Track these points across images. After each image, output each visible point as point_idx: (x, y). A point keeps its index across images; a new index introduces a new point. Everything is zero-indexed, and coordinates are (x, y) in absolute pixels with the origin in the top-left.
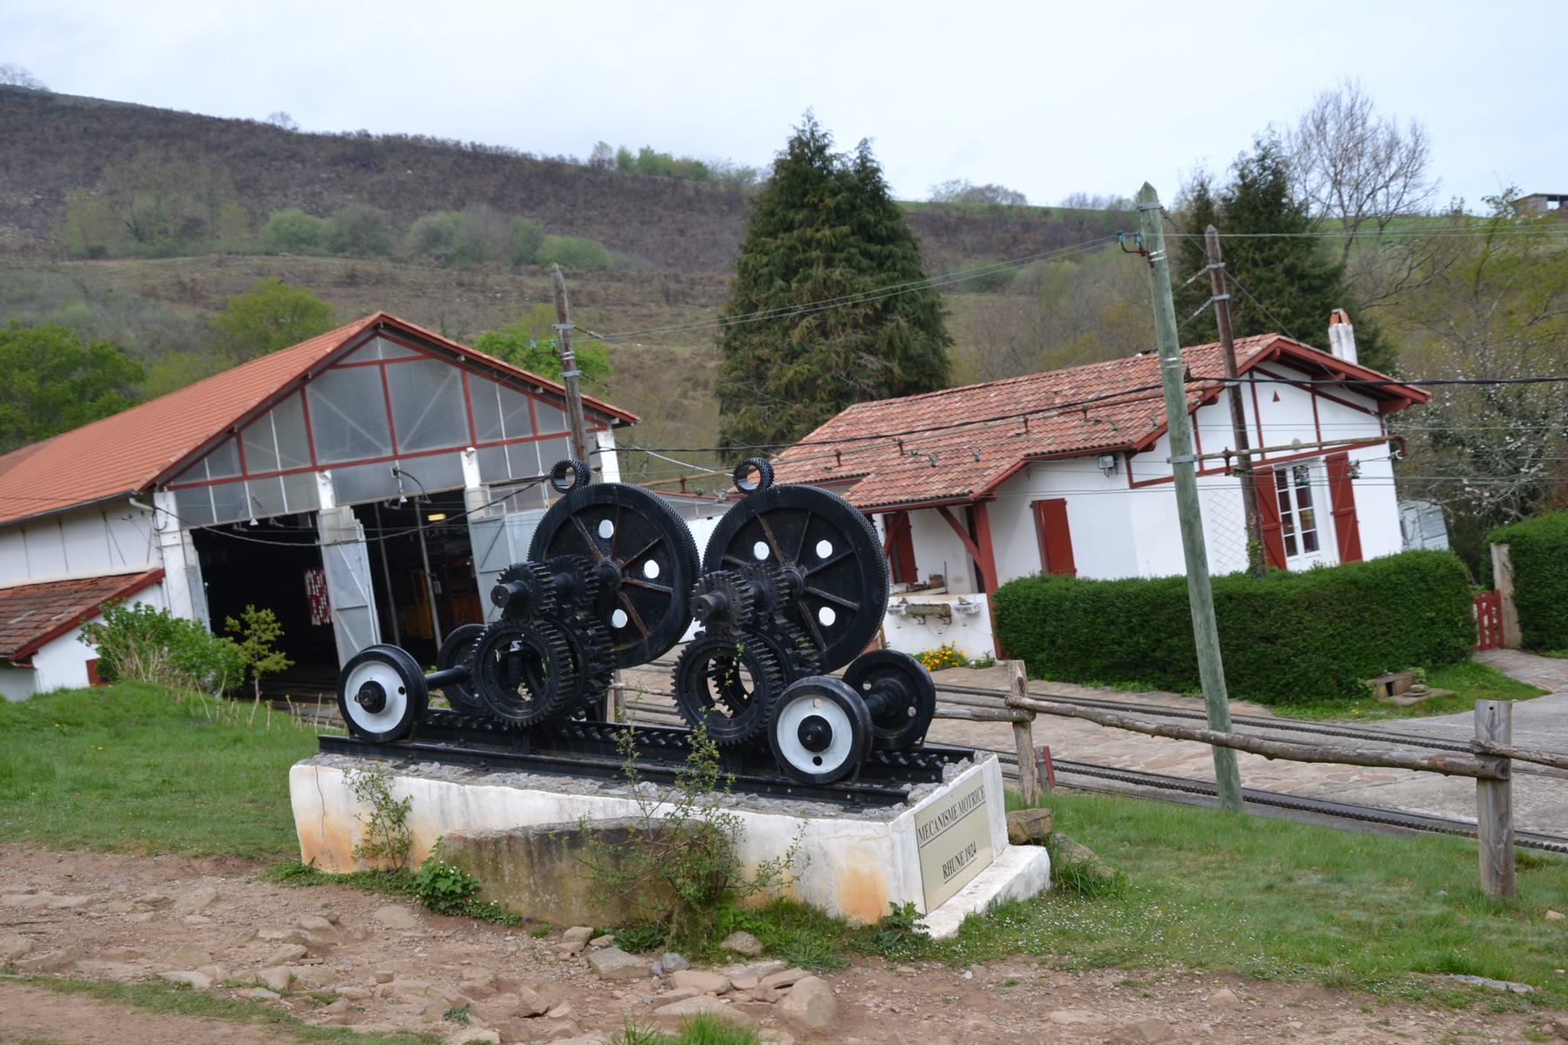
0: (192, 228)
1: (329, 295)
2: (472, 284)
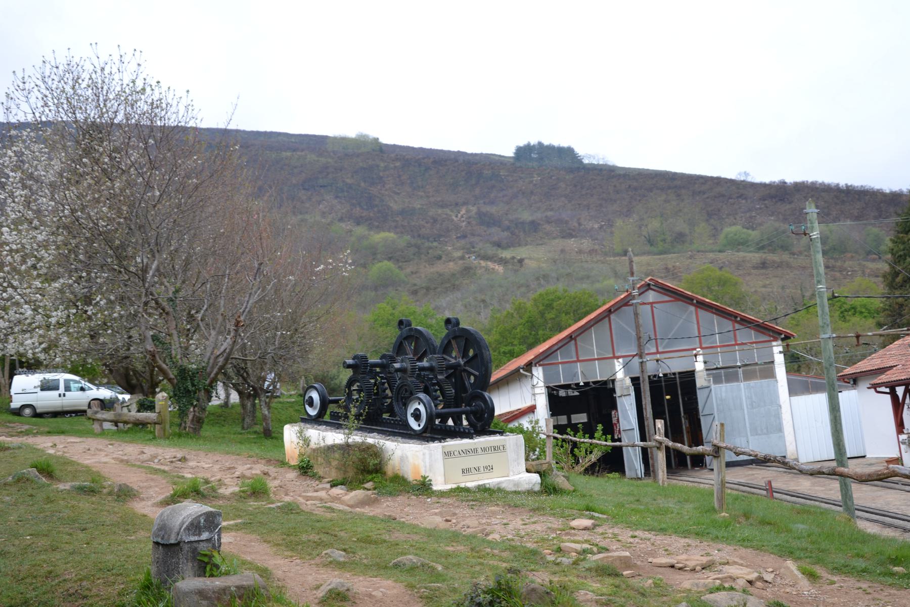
0: (680, 238)
1: (749, 274)
2: (834, 267)
